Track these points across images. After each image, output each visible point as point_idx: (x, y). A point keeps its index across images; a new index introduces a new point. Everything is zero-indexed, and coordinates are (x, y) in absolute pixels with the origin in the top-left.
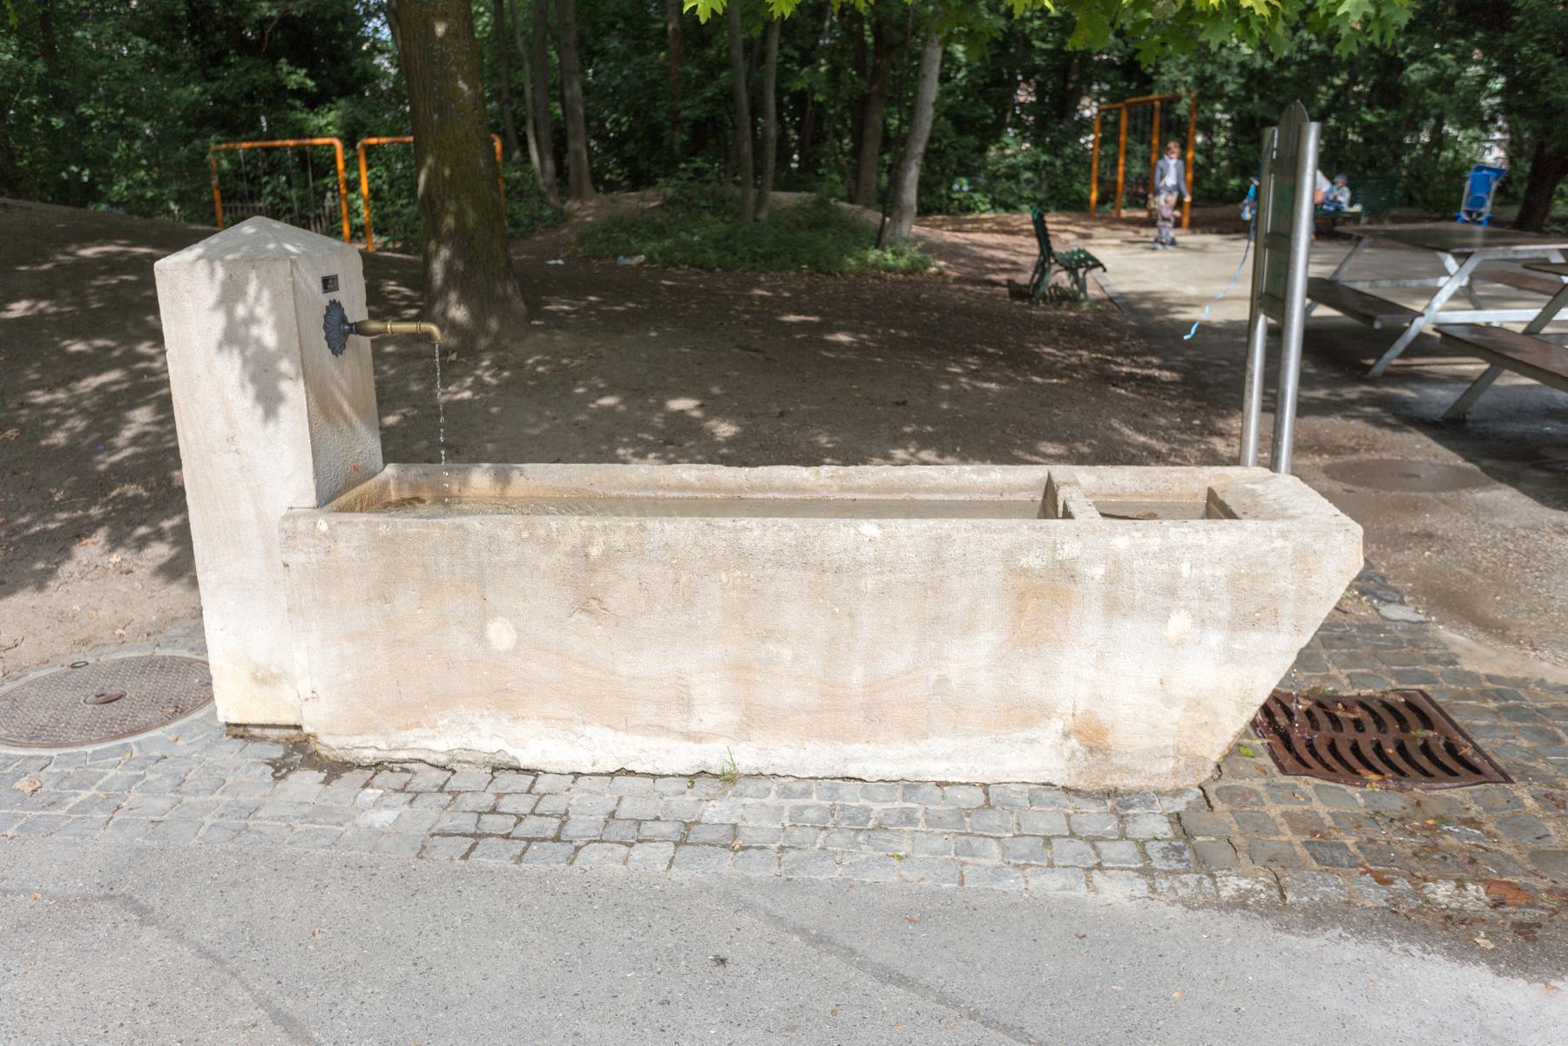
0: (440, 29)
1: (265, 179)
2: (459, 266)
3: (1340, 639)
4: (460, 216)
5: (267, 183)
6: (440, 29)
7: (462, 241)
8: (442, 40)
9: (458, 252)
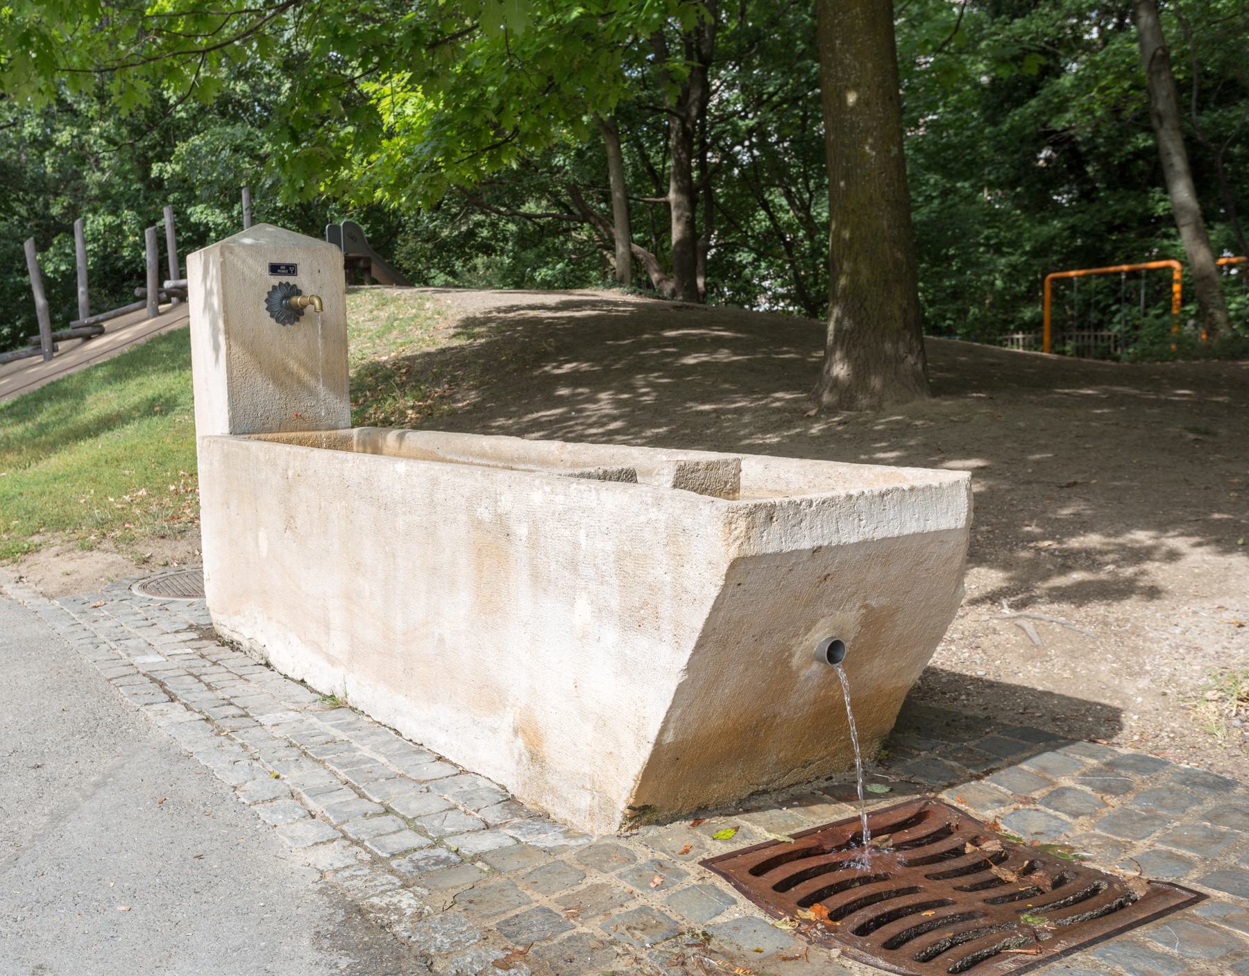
0: (851, 98)
1: (1114, 308)
2: (847, 324)
3: (114, 69)
4: (854, 274)
5: (1118, 311)
6: (851, 98)
7: (855, 302)
8: (853, 109)
9: (847, 311)
